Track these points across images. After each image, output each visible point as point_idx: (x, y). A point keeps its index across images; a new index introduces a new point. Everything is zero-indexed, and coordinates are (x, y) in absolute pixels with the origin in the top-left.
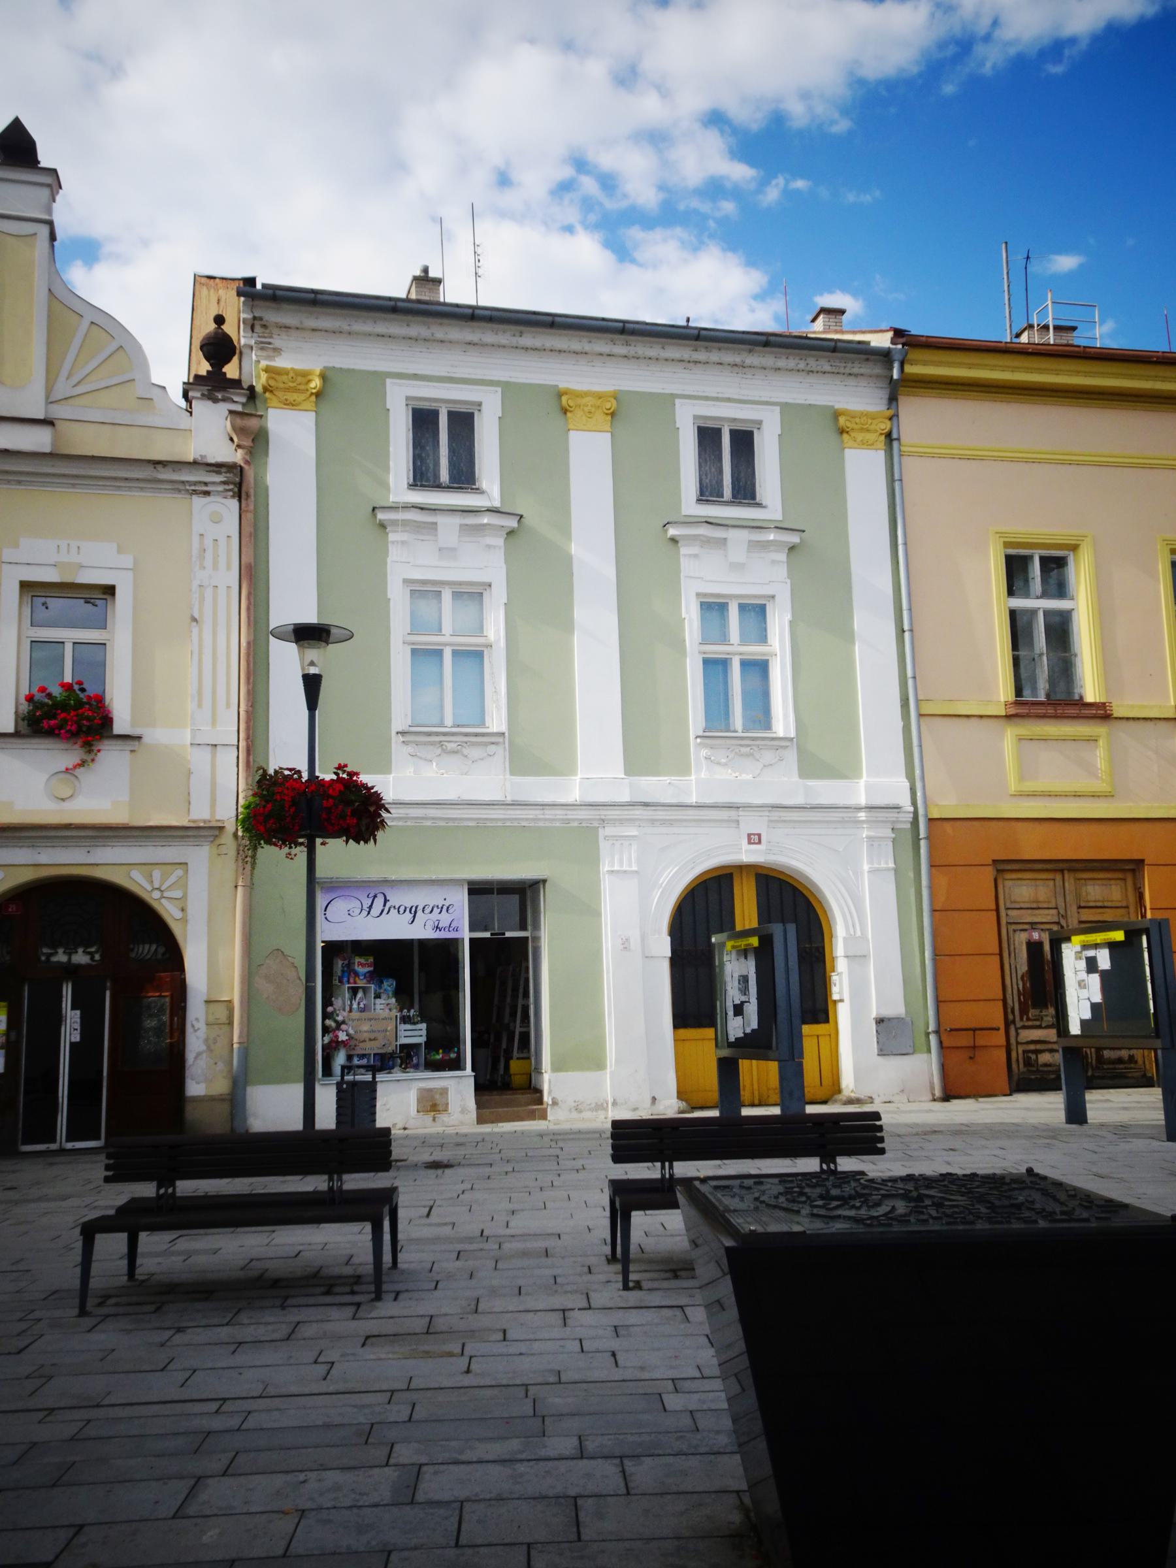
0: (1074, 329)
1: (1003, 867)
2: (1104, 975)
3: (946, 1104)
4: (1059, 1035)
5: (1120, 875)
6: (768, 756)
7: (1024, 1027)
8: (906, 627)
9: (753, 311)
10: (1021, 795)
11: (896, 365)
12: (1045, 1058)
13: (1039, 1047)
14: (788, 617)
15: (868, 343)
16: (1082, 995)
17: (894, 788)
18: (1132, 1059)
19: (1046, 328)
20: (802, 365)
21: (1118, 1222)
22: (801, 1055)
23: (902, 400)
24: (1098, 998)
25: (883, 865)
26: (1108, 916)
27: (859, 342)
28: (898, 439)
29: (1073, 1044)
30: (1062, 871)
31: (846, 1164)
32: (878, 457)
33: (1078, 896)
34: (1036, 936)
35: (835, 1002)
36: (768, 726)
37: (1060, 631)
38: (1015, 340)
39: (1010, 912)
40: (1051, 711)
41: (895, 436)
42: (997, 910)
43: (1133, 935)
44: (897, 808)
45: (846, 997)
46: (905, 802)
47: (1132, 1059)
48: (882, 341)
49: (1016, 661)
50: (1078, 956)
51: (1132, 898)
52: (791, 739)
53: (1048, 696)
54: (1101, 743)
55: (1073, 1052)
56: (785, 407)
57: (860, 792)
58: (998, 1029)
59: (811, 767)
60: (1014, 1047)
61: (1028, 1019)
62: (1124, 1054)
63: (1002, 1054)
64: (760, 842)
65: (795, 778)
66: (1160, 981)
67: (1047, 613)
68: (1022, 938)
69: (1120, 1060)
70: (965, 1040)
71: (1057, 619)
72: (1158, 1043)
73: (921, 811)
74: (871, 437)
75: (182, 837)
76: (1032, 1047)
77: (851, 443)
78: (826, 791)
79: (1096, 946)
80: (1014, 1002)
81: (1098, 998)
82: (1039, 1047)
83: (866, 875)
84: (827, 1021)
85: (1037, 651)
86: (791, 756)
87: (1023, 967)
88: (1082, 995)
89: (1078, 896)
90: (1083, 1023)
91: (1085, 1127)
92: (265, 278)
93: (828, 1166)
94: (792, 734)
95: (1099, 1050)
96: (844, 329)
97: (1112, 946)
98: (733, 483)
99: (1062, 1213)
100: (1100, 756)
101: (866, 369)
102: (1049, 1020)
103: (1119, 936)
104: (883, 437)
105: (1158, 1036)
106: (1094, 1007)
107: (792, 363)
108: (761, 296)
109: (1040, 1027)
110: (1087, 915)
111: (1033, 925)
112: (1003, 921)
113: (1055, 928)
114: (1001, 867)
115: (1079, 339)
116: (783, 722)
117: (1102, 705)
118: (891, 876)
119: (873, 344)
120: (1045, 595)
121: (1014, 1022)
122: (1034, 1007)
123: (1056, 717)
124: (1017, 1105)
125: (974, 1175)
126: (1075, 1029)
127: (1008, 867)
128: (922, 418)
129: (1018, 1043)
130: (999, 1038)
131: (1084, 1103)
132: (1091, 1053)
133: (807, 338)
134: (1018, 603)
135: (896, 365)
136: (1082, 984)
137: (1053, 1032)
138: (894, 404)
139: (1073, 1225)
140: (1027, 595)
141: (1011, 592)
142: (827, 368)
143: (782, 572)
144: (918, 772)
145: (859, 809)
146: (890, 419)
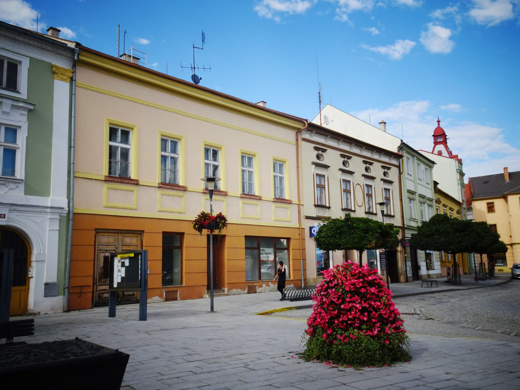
0: (139, 59)
1: (98, 231)
2: (127, 268)
3: (68, 313)
4: (110, 288)
5: (136, 235)
6: (12, 186)
7: (99, 285)
8: (72, 146)
9: (32, 25)
10: (160, 211)
11: (76, 55)
12: (106, 295)
13: (104, 292)
14: (26, 135)
15: (67, 44)
16: (119, 274)
17: (63, 202)
18: (133, 294)
19: (130, 56)
20: (40, 45)
21: (98, 354)
22: (10, 299)
23: (78, 67)
24: (123, 275)
25: (55, 228)
26: (131, 248)
27: (63, 43)
28: (75, 80)
29: (114, 290)
30: (118, 233)
31: (16, 339)
32: (67, 85)
33: (122, 241)
34: (107, 254)
35: (30, 278)
36: (13, 174)
37: (125, 154)
38: (120, 58)
39: (99, 246)
40: (120, 180)
41: (74, 79)
42: (95, 246)
43: (137, 255)
44: (62, 208)
45: (34, 276)
46: (66, 206)
47: (133, 294)
48: (72, 45)
49: (110, 163)
50: (119, 261)
51: (139, 243)
52: (23, 180)
53: (119, 175)
54: (135, 192)
55: (114, 293)
56: (32, 59)
57: (48, 202)
58: (90, 286)
59: (28, 191)
60: (95, 292)
61: (101, 282)
62: (131, 293)
63: (91, 295)
64: (4, 218)
65: (22, 194)
66: (143, 269)
67: (122, 148)
68: (102, 255)
69: (130, 295)
70: (78, 290)
71: (125, 151)
72: (140, 289)
73: (71, 210)
74: (65, 77)
75: (40, 212)
76: (102, 292)
77: (57, 78)
78: (34, 200)
79: (125, 258)
80: (97, 276)
81: (123, 275)
82: (104, 292)
83: (47, 232)
84: (25, 285)
85: (117, 160)
86: (22, 187)
87: (101, 264)
88: (119, 274)
89: (122, 241)
90: (118, 283)
91: (115, 318)
92: (84, 44)
93: (10, 341)
94: (23, 178)
95: (123, 292)
96: (60, 37)
97: (130, 258)
98: (7, 82)
99: (81, 353)
100: (134, 196)
101: (65, 53)
102: (108, 282)
103: (132, 255)
104: (69, 79)
105: (140, 287)
106: (122, 278)
107: (36, 44)
108: (37, 21)
109: (105, 285)
110: (125, 248)
111: (107, 251)
112: (97, 249)
113: (114, 252)
114: (98, 231)
115: (140, 63)
116: (20, 172)
117: (137, 181)
118: (58, 232)
119: (68, 45)
120: (121, 142)
121: (96, 283)
122: (104, 278)
123: (121, 182)
124: (94, 312)
125: (56, 341)
126: (115, 285)
127: (100, 231)
128: (84, 76)
129: (97, 291)
130: (91, 289)
131: (115, 310)
132: (121, 293)
133: (42, 36)
134: (112, 143)
135: (76, 55)
136: (119, 271)
137: (108, 286)
138: (74, 68)
139: (83, 357)
140: (115, 141)
141: (110, 140)
142: (50, 49)
143: (25, 118)
144: (71, 196)
145: (47, 207)
146: (73, 73)
